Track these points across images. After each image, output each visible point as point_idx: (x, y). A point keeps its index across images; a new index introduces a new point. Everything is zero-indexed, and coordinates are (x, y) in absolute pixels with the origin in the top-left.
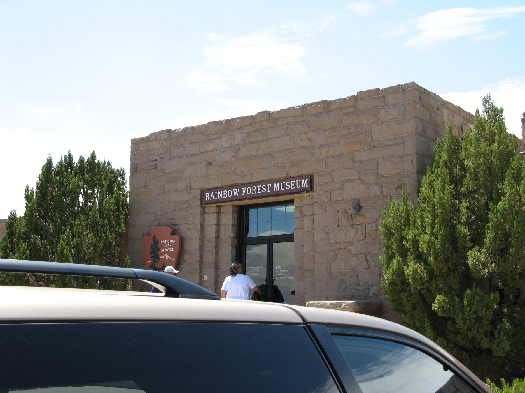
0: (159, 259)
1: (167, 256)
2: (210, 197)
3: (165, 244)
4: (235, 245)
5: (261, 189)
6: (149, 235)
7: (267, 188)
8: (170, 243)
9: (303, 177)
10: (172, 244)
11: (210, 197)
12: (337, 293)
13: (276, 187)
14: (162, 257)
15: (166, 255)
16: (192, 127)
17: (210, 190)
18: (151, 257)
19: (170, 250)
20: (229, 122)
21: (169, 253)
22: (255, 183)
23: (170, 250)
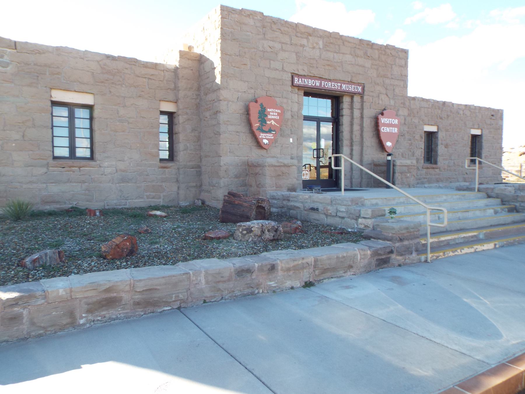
0: (266, 123)
1: (273, 123)
2: (298, 81)
3: (272, 112)
4: (340, 117)
5: (334, 86)
6: (256, 102)
7: (338, 86)
8: (275, 112)
9: (359, 84)
10: (278, 113)
11: (298, 81)
12: (156, 216)
13: (344, 86)
14: (268, 122)
15: (272, 121)
16: (57, 47)
17: (299, 76)
18: (259, 121)
19: (276, 117)
20: (315, 30)
21: (275, 120)
22: (330, 80)
23: (276, 117)
